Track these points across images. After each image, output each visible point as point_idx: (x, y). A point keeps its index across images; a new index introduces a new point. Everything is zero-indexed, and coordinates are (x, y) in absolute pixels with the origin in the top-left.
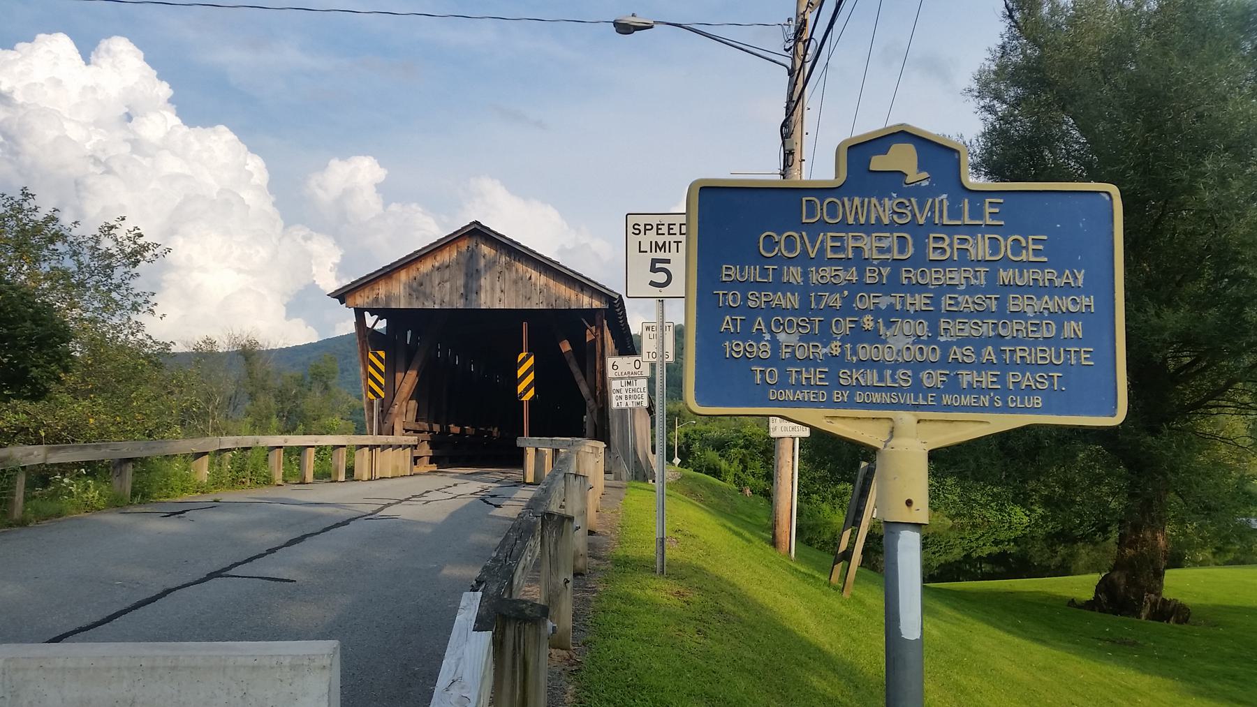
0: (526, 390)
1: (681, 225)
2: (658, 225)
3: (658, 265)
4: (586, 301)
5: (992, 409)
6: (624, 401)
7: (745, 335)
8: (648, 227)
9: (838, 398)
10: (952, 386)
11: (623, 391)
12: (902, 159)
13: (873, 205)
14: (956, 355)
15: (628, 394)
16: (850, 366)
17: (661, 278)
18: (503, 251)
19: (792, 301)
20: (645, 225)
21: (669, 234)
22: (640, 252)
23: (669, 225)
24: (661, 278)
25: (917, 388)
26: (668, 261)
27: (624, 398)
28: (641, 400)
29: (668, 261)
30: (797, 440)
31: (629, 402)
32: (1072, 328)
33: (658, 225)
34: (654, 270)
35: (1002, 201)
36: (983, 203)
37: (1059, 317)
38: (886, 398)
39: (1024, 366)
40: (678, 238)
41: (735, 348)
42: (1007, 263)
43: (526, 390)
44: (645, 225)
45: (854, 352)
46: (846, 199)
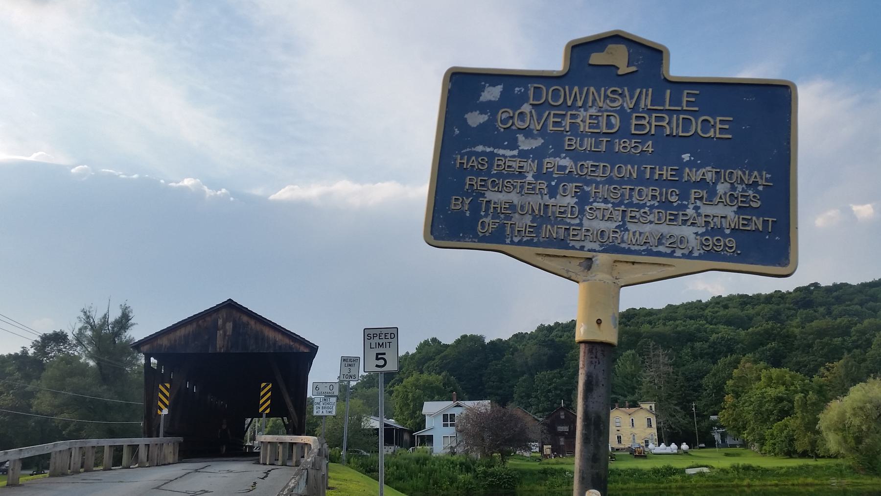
1: (391, 334)
2: (379, 334)
3: (379, 356)
4: (303, 349)
6: (321, 410)
8: (375, 335)
11: (321, 403)
13: (591, 93)
14: (722, 199)
15: (324, 406)
17: (381, 362)
20: (374, 334)
21: (385, 338)
22: (371, 348)
23: (385, 334)
24: (381, 362)
26: (384, 354)
27: (321, 408)
28: (331, 410)
29: (384, 354)
31: (324, 411)
33: (379, 334)
34: (377, 359)
35: (697, 92)
36: (682, 94)
40: (390, 340)
44: (374, 334)
46: (567, 88)
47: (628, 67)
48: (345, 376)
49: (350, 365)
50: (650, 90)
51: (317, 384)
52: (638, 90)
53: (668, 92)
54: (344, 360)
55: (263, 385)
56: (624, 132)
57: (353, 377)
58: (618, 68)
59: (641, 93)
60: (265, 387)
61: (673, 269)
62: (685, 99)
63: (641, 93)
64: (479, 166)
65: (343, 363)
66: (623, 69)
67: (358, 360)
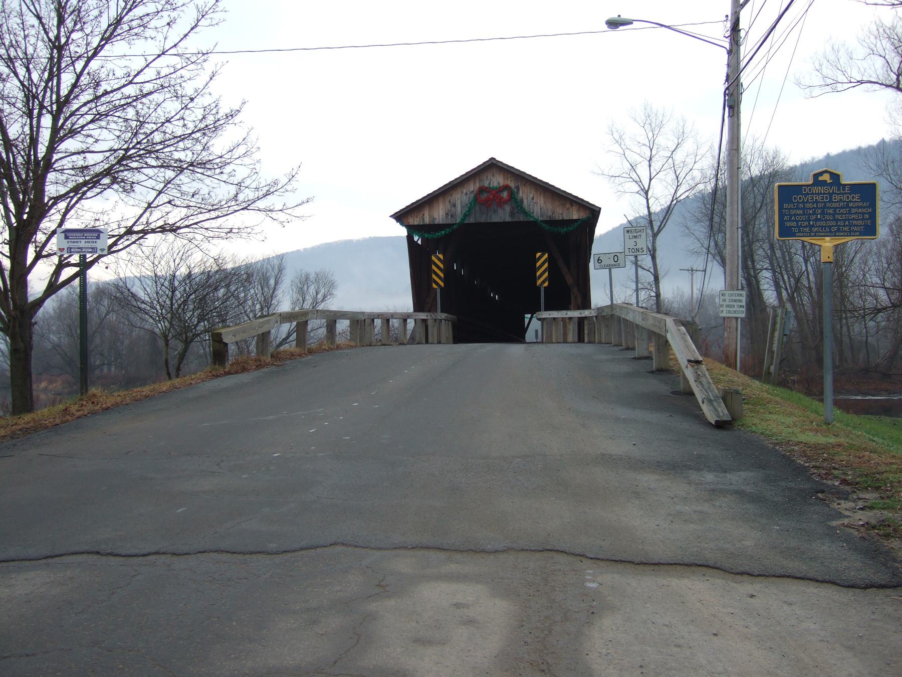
0: (542, 279)
5: (847, 236)
7: (790, 220)
9: (836, 199)
10: (838, 230)
12: (826, 177)
16: (815, 227)
18: (512, 178)
19: (801, 212)
25: (830, 232)
30: (739, 320)
32: (867, 216)
37: (863, 214)
38: (823, 234)
39: (855, 225)
41: (788, 224)
42: (851, 201)
43: (542, 279)
45: (816, 224)
47: (390, 216)
48: (630, 250)
49: (635, 237)
51: (599, 255)
54: (628, 231)
55: (538, 255)
56: (831, 201)
57: (640, 250)
60: (540, 257)
65: (627, 235)
66: (829, 182)
67: (645, 231)
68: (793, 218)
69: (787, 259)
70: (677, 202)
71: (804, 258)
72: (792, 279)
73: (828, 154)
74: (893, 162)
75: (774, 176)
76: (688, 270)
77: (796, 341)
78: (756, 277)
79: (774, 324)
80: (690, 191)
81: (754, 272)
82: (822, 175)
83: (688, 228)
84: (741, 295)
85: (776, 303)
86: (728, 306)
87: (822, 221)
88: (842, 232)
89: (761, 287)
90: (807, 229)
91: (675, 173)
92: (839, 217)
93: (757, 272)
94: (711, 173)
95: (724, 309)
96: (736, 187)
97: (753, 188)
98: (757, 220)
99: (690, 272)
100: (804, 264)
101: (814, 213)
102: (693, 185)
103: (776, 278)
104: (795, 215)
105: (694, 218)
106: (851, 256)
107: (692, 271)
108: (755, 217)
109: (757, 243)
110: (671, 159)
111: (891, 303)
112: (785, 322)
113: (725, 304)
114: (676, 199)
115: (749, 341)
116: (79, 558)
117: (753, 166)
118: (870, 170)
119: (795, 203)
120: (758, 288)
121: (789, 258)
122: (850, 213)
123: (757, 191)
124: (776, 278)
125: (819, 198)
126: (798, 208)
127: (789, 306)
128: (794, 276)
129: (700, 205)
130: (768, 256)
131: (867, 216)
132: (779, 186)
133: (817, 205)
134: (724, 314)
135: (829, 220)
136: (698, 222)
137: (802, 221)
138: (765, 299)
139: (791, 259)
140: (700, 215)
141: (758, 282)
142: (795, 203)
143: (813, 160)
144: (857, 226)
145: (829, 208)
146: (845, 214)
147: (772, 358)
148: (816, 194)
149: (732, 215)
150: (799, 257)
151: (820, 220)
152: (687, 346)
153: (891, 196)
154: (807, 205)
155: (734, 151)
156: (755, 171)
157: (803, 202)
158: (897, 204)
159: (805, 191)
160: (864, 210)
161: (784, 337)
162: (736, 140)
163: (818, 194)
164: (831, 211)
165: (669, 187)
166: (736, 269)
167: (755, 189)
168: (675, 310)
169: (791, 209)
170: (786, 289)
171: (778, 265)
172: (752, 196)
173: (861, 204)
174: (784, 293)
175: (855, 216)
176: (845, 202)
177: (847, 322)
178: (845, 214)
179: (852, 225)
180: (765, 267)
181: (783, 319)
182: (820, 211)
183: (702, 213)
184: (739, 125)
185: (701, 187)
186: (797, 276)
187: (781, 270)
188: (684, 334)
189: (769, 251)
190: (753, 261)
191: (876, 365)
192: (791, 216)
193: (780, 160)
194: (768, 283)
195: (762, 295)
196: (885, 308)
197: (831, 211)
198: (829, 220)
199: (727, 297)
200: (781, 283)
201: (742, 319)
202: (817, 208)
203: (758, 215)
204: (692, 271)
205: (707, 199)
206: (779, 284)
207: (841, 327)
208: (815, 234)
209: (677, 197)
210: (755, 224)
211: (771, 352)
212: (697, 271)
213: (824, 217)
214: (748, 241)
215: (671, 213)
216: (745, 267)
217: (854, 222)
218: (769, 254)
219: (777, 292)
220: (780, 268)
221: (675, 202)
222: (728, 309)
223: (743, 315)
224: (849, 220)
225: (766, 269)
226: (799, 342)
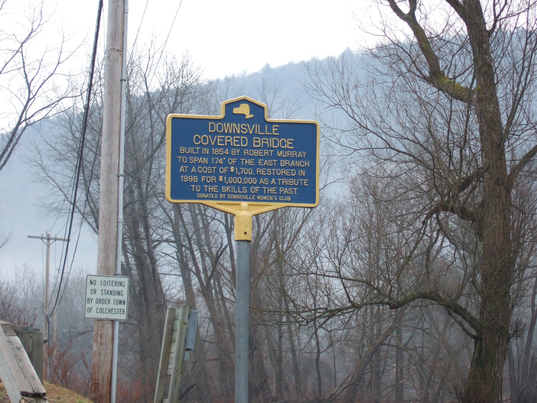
5: (273, 201)
7: (189, 173)
9: (257, 144)
10: (261, 192)
12: (244, 110)
16: (225, 185)
19: (205, 160)
25: (249, 193)
32: (303, 172)
37: (297, 168)
38: (238, 197)
39: (285, 186)
41: (185, 178)
42: (280, 149)
45: (227, 180)
46: (224, 124)
50: (256, 133)
52: (254, 125)
53: (266, 126)
56: (250, 146)
58: (245, 116)
59: (255, 126)
61: (272, 207)
62: (274, 129)
63: (255, 126)
64: (242, 131)
66: (248, 116)
68: (193, 170)
69: (201, 226)
70: (27, 125)
71: (226, 226)
72: (207, 258)
73: (267, 66)
74: (356, 86)
75: (184, 94)
76: (42, 238)
77: (210, 358)
78: (150, 254)
79: (171, 331)
80: (49, 109)
81: (148, 245)
82: (238, 106)
83: (44, 169)
84: (121, 284)
85: (182, 296)
86: (99, 301)
87: (237, 176)
88: (265, 195)
89: (160, 270)
90: (214, 188)
91: (26, 77)
92: (262, 172)
93: (152, 245)
94: (83, 81)
95: (93, 305)
96: (118, 110)
97: (150, 111)
98: (156, 162)
99: (45, 241)
100: (225, 235)
101: (225, 164)
102: (55, 100)
103: (182, 256)
104: (197, 164)
105: (55, 153)
106: (296, 226)
107: (49, 239)
108: (151, 158)
109: (154, 199)
110: (19, 54)
111: (350, 301)
112: (187, 329)
113: (94, 297)
114: (26, 120)
115: (138, 356)
116: (328, 79)
117: (151, 75)
118: (324, 97)
119: (198, 146)
120: (154, 270)
121: (204, 224)
122: (278, 166)
123: (155, 116)
124: (182, 256)
125: (233, 141)
126: (200, 155)
127: (200, 301)
128: (210, 254)
129: (64, 131)
130: (171, 221)
131: (303, 172)
132: (174, 119)
133: (230, 151)
134: (93, 314)
135: (248, 176)
136: (60, 160)
137: (207, 174)
138: (164, 289)
139: (206, 226)
140: (65, 148)
141: (154, 262)
142: (198, 146)
143: (245, 72)
144: (288, 186)
145: (248, 157)
146: (271, 167)
147: (167, 385)
148: (228, 134)
149: (110, 155)
150: (218, 223)
151: (233, 174)
152: (22, 369)
153: (354, 138)
154: (216, 151)
155: (116, 54)
156: (154, 86)
157: (209, 146)
158: (361, 151)
159: (212, 129)
160: (299, 164)
161: (187, 352)
162: (120, 34)
163: (232, 135)
164: (250, 162)
165: (15, 100)
166: (113, 242)
167: (153, 112)
168: (19, 302)
169: (190, 155)
170: (198, 274)
171: (187, 234)
172: (148, 123)
173: (293, 154)
174: (195, 280)
175: (286, 172)
176: (272, 148)
177: (290, 328)
178: (271, 167)
179: (281, 185)
180: (165, 237)
181: (185, 324)
182: (234, 161)
183: (68, 145)
184: (125, 13)
185: (67, 103)
186: (215, 253)
187: (190, 243)
188: (19, 349)
189: (173, 212)
190: (147, 228)
191: (331, 396)
192: (190, 166)
193: (193, 70)
194: (169, 264)
195: (160, 282)
196: (341, 310)
197: (250, 162)
198: (248, 176)
199: (98, 287)
200: (191, 265)
201: (122, 323)
202: (230, 156)
203: (156, 155)
204: (49, 239)
205: (77, 124)
206: (187, 265)
207: (281, 337)
208: (226, 196)
209: (28, 117)
210: (151, 168)
211: (165, 375)
212: (56, 239)
213: (240, 171)
214: (141, 194)
215: (16, 143)
216: (134, 237)
217: (284, 181)
218: (173, 217)
219: (184, 279)
220: (189, 239)
221: (23, 124)
222: (100, 306)
223: (124, 317)
224: (276, 176)
225: (167, 241)
226: (216, 360)
